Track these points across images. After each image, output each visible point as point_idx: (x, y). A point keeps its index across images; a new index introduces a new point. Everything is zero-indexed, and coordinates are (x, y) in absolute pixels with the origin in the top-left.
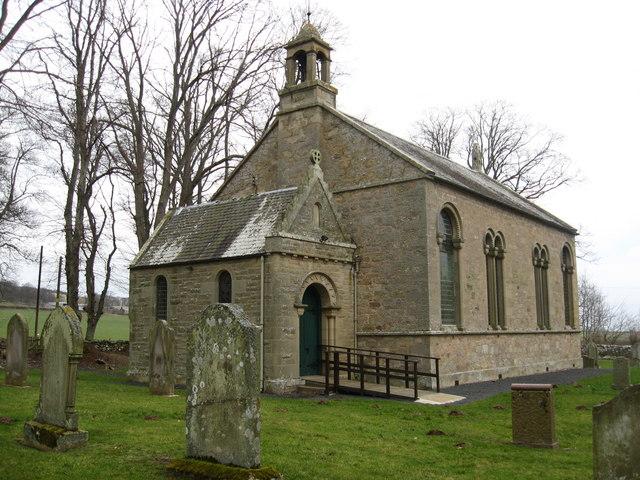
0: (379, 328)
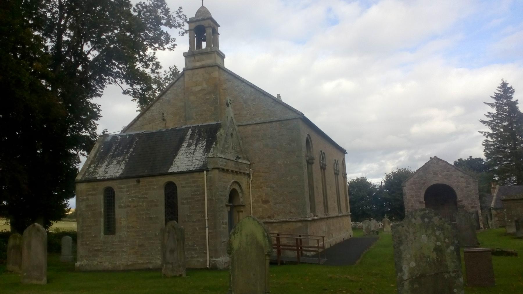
0: (269, 217)
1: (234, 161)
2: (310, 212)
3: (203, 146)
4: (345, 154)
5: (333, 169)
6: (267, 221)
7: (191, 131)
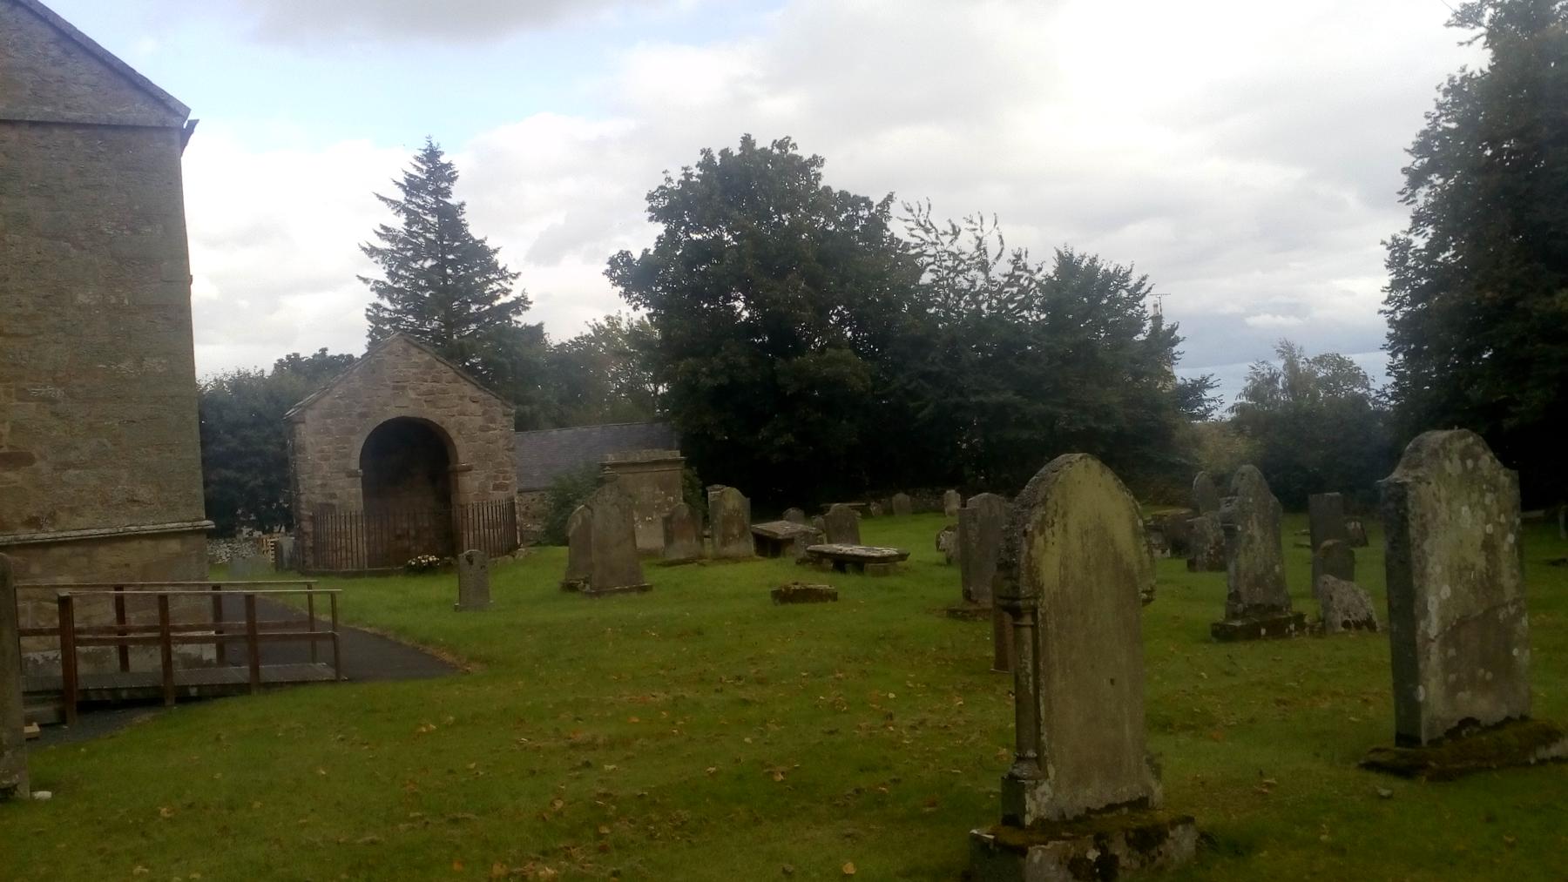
0: (33, 522)
6: (22, 537)
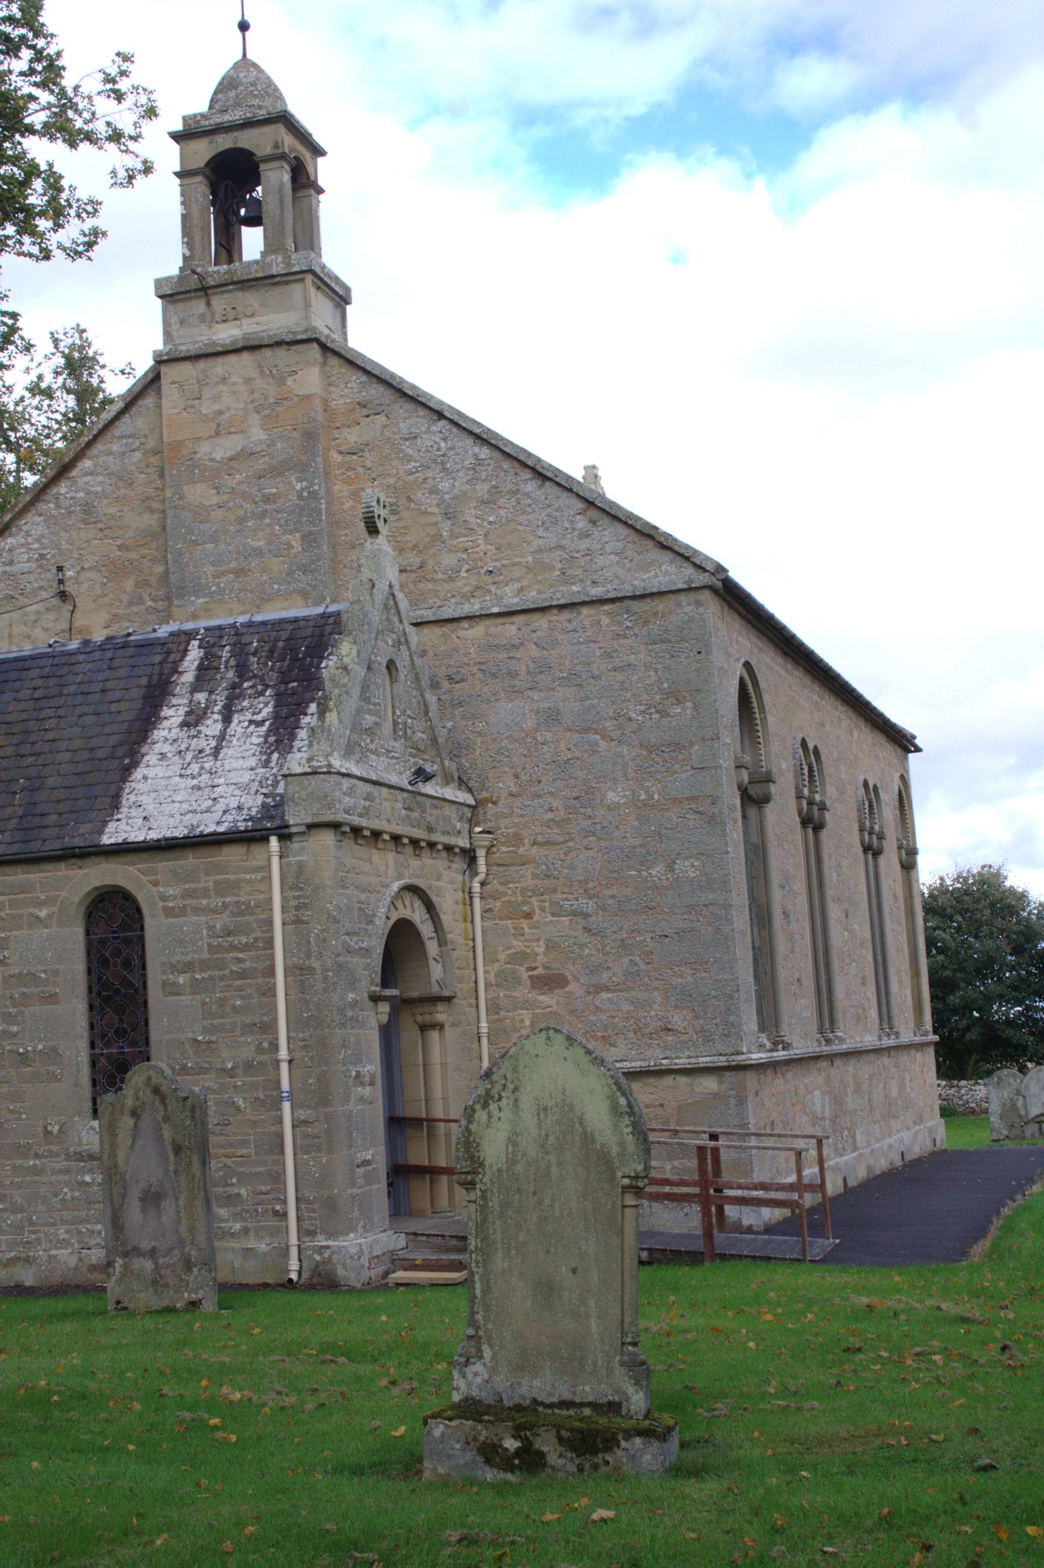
1: (402, 790)
2: (756, 1029)
3: (261, 723)
4: (910, 755)
5: (856, 828)
7: (202, 651)
